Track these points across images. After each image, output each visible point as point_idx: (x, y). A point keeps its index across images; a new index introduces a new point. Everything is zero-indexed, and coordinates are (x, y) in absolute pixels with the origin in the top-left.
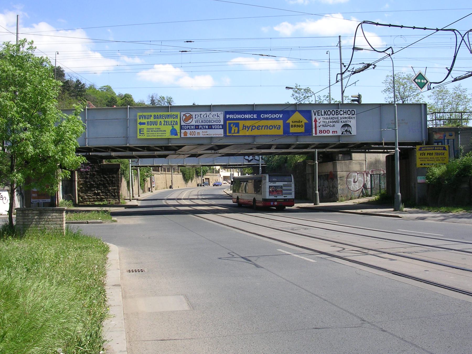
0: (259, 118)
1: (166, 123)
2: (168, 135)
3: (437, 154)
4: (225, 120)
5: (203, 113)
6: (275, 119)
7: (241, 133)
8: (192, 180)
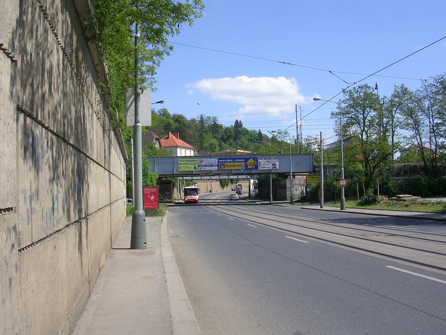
0: (234, 162)
1: (192, 164)
2: (192, 169)
3: (317, 178)
4: (218, 162)
5: (208, 159)
6: (241, 162)
7: (226, 168)
8: (227, 185)
